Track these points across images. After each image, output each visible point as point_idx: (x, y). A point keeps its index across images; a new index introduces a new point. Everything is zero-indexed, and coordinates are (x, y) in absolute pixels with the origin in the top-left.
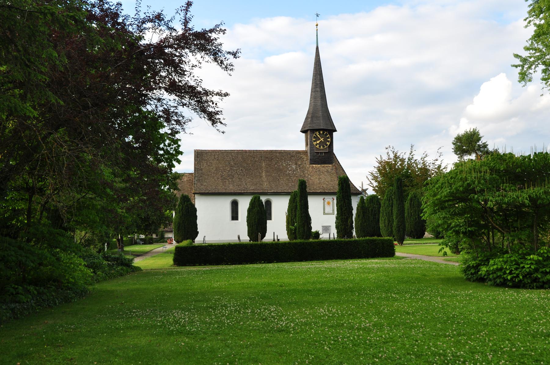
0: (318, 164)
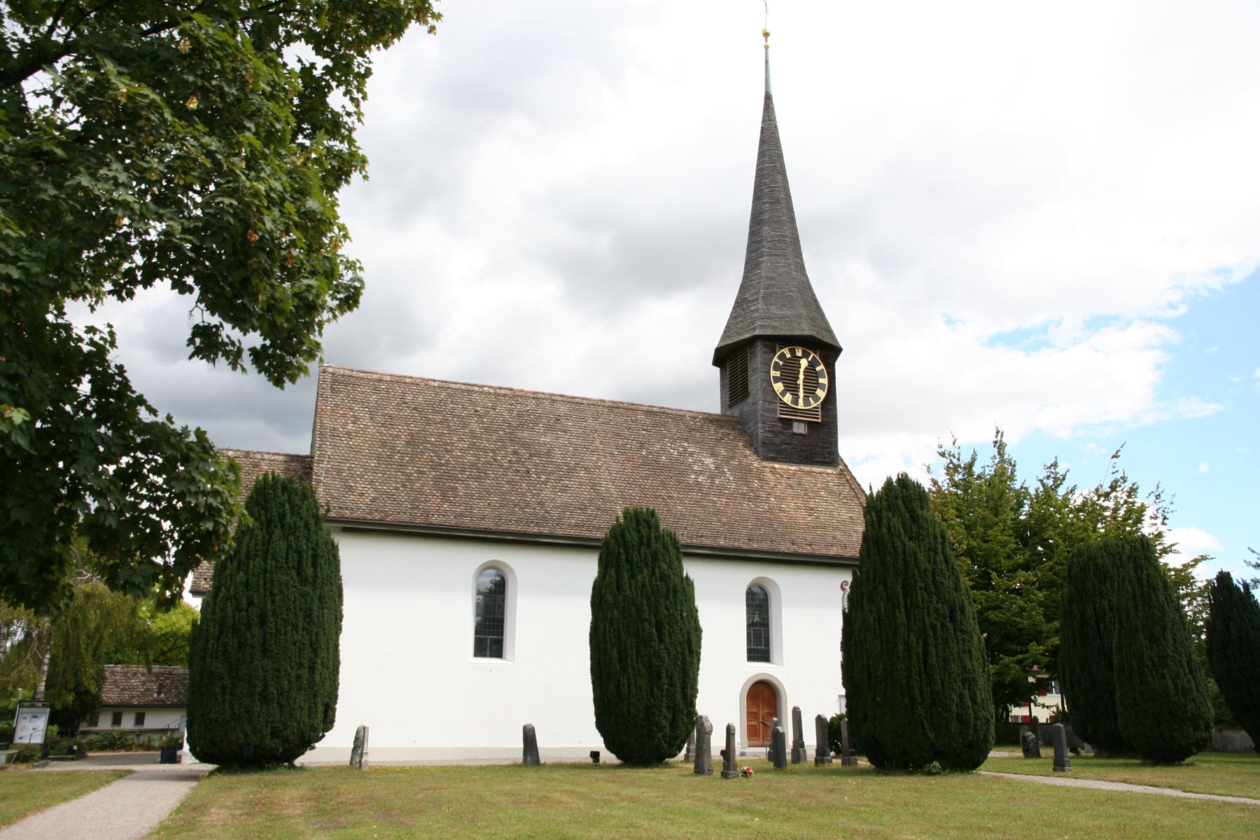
0: (790, 461)
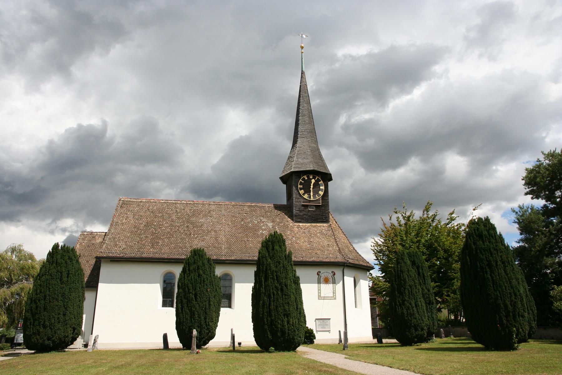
0: (307, 221)
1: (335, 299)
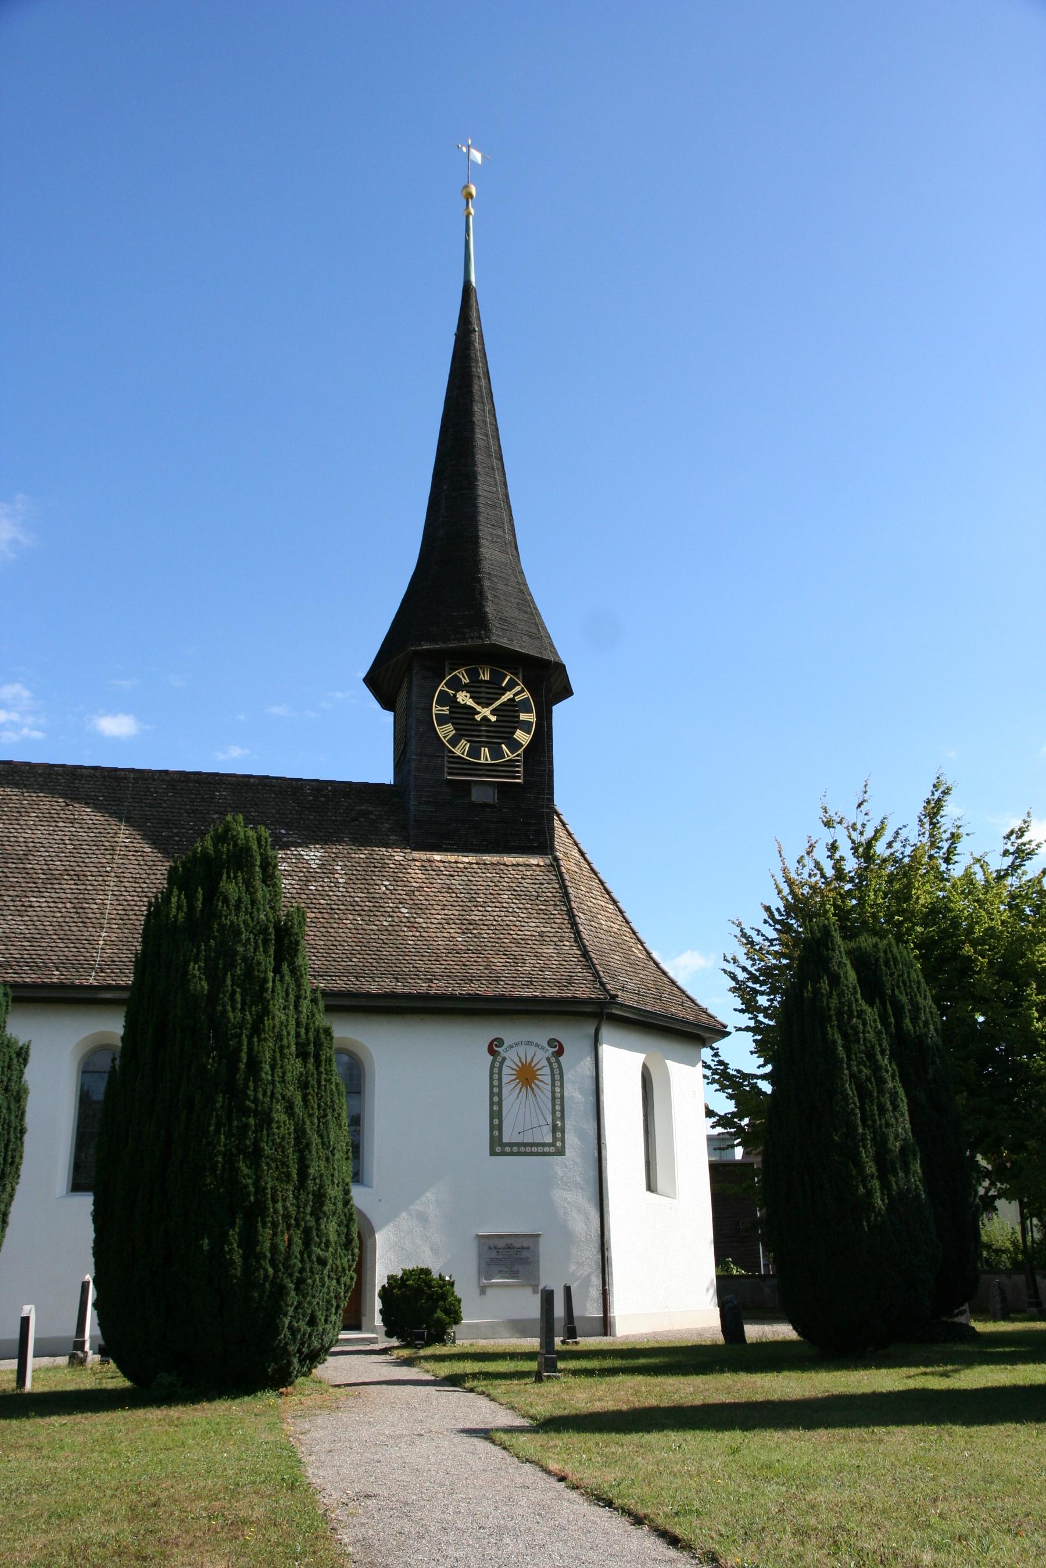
1: (493, 1153)
